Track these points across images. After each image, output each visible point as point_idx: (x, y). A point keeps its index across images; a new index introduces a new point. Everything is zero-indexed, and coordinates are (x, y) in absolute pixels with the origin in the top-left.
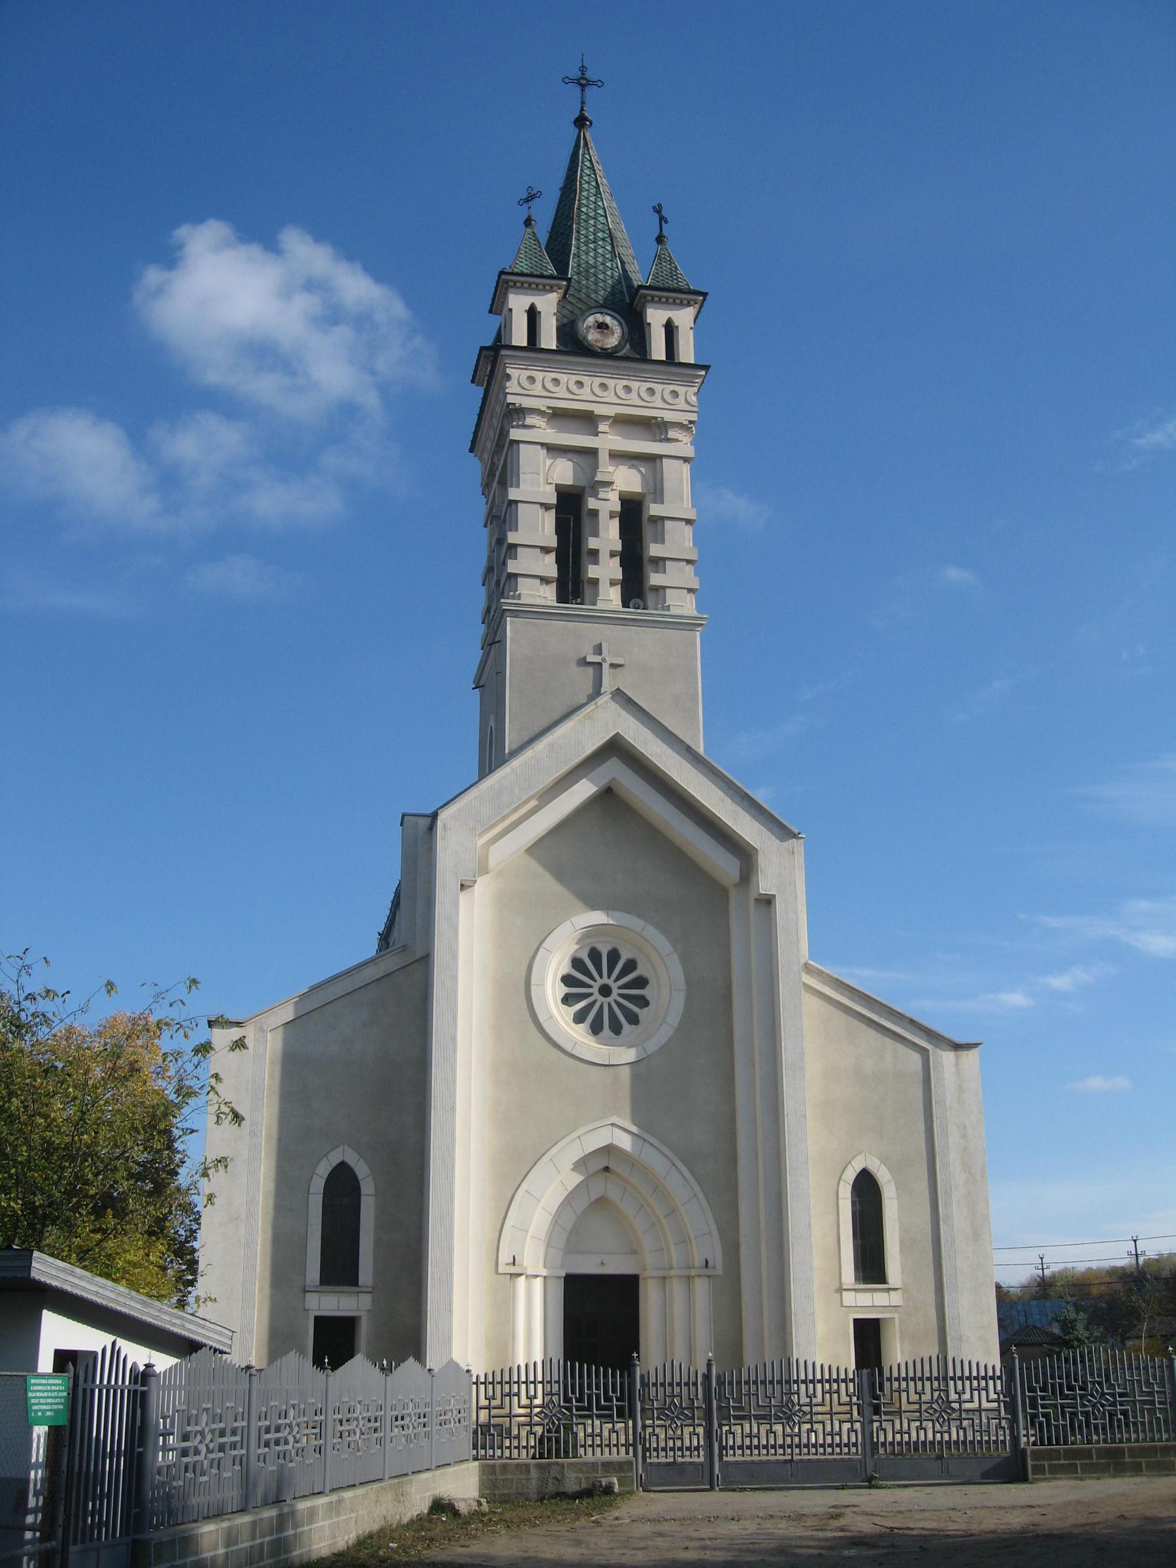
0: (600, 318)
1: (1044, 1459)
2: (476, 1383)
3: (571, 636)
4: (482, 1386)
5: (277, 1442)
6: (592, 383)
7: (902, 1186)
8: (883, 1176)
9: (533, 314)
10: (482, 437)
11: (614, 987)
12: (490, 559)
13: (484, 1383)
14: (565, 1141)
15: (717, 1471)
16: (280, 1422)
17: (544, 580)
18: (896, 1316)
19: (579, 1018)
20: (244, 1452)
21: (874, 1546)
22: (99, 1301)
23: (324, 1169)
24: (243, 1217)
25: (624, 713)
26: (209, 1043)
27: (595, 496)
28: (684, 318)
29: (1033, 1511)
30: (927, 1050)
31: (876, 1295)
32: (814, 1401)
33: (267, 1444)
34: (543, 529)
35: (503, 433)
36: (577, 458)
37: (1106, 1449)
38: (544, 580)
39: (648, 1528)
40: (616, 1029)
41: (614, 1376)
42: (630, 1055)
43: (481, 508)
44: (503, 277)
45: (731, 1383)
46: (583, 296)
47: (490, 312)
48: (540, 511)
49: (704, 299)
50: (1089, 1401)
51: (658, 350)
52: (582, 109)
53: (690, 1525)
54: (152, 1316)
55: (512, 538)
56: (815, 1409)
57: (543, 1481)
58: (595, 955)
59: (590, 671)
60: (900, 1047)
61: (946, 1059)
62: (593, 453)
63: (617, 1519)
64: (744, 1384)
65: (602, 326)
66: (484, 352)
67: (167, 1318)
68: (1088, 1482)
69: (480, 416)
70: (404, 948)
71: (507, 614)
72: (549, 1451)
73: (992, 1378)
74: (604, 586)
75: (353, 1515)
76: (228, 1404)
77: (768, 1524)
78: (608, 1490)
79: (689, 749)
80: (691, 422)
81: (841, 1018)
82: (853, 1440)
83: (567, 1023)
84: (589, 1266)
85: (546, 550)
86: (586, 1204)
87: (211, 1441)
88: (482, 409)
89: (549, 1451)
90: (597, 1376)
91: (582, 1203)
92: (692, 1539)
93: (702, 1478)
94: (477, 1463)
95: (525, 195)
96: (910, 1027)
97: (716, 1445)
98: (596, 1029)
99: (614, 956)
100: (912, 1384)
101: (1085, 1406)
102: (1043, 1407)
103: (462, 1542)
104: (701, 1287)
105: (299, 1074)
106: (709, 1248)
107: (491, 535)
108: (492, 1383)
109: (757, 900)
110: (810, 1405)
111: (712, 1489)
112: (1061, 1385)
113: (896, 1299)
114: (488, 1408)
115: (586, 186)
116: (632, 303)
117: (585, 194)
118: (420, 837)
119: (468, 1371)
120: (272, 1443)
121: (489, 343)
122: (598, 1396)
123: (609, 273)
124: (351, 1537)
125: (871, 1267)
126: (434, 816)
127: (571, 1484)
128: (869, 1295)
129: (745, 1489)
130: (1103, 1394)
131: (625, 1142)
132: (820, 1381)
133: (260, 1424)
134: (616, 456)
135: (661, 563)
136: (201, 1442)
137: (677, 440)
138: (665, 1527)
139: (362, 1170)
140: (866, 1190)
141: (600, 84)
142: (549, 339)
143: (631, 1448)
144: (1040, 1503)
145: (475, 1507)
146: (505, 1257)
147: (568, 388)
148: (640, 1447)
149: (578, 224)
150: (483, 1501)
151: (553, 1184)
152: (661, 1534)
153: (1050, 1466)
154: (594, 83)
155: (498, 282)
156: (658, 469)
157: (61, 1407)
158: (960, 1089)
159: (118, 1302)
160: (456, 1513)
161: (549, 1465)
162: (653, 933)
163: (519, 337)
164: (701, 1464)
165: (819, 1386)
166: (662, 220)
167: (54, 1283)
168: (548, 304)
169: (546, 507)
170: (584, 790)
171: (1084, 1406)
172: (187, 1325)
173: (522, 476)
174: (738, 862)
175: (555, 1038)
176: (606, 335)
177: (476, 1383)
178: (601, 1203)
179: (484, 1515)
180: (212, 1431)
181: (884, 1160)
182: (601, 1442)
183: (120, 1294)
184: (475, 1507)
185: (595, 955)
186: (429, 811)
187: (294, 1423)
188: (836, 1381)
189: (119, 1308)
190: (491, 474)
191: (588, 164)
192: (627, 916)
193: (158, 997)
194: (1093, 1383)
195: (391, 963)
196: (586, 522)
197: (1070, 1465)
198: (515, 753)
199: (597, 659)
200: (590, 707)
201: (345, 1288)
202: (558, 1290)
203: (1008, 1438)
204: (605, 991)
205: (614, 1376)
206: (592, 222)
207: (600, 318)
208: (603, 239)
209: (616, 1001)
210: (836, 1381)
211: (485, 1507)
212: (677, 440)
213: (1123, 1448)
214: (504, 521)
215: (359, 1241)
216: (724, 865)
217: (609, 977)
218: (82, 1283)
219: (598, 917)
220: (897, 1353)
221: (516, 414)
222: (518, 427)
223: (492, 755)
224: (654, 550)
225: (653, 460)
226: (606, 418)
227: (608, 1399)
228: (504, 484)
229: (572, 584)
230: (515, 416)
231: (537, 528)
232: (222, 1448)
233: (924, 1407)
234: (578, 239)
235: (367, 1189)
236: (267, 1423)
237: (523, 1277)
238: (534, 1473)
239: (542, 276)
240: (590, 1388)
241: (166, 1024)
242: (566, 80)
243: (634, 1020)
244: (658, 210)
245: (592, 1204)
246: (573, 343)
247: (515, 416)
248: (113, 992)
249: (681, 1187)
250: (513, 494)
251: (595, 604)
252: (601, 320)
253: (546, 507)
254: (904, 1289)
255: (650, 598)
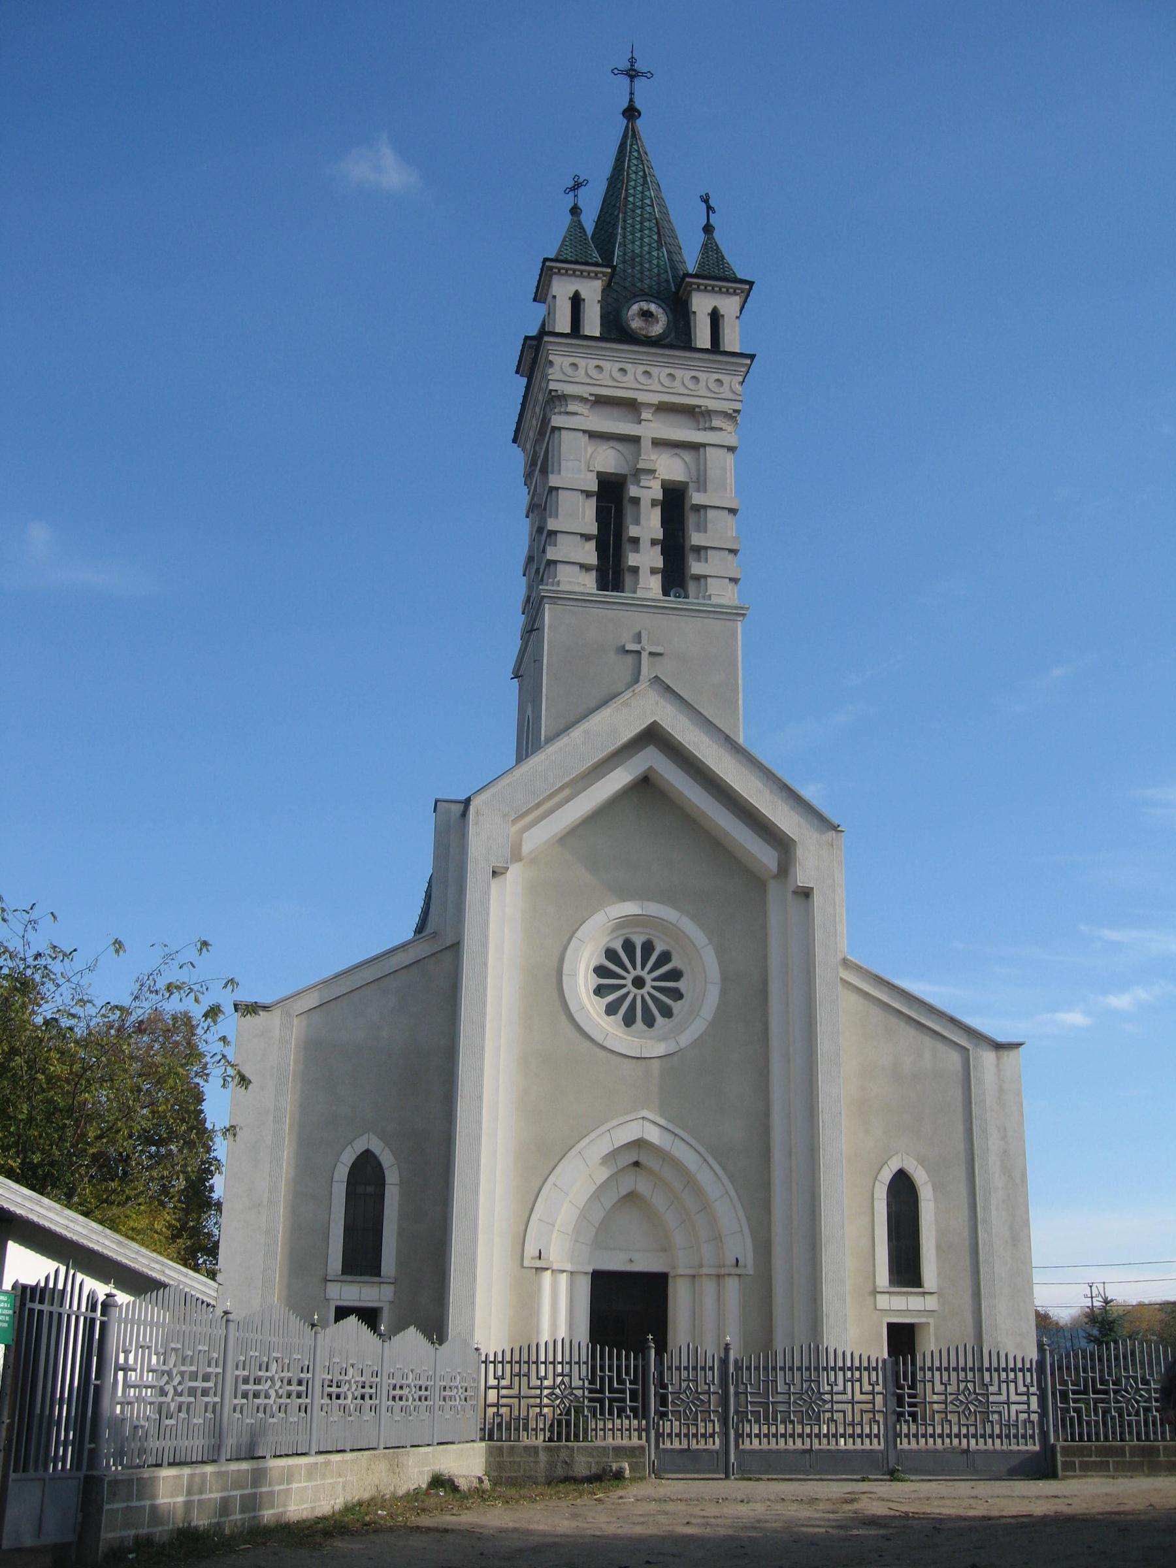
0: (645, 306)
1: (1074, 1455)
2: (485, 1362)
3: (613, 622)
4: (492, 1365)
5: (256, 1395)
6: (635, 372)
7: (939, 1188)
8: (920, 1177)
9: (577, 301)
10: (525, 425)
11: (648, 978)
12: (531, 548)
13: (493, 1362)
14: (593, 1135)
15: (732, 1459)
16: (260, 1373)
17: (585, 567)
18: (931, 1320)
19: (611, 1010)
20: (217, 1399)
21: (885, 1526)
22: (69, 1235)
23: (348, 1158)
24: (265, 1203)
25: (662, 701)
26: (218, 1007)
27: (638, 483)
28: (729, 305)
29: (1057, 1501)
30: (967, 1050)
31: (911, 1299)
32: (835, 1389)
33: (245, 1395)
34: (584, 517)
35: (545, 421)
36: (619, 446)
37: (1139, 1446)
38: (585, 567)
39: (653, 1506)
40: (650, 1022)
41: (627, 1358)
42: (660, 1049)
43: (522, 498)
44: (548, 264)
45: (749, 1368)
46: (627, 284)
47: (535, 300)
48: (581, 497)
49: (751, 288)
50: (1122, 1396)
51: (703, 339)
52: (631, 100)
53: (696, 1505)
54: (127, 1257)
55: (552, 525)
56: (836, 1398)
57: (552, 1465)
58: (628, 946)
59: (630, 660)
60: (941, 1047)
61: (988, 1057)
62: (636, 440)
63: (621, 1498)
64: (770, 1385)
65: (646, 315)
66: (528, 342)
67: (144, 1261)
68: (1120, 1480)
69: (523, 405)
70: (435, 935)
71: (545, 600)
72: (560, 1434)
73: (1021, 1370)
74: (644, 573)
75: (341, 1480)
76: (200, 1348)
77: (778, 1506)
78: (618, 1476)
79: (727, 738)
80: (735, 411)
81: (877, 1014)
82: (876, 1431)
83: (599, 1015)
84: (616, 1262)
85: (586, 537)
86: (616, 1199)
87: (180, 1383)
88: (525, 397)
89: (560, 1434)
90: (610, 1358)
91: (612, 1198)
92: (695, 1517)
93: (718, 1465)
94: (483, 1444)
95: (571, 184)
96: (951, 1026)
97: (732, 1432)
98: (629, 1021)
99: (648, 947)
100: (937, 1374)
101: (1119, 1402)
102: (1075, 1401)
103: (454, 1512)
104: (732, 1287)
105: (322, 1060)
106: (739, 1246)
107: (532, 525)
108: (502, 1362)
109: (795, 893)
110: (831, 1393)
111: (727, 1477)
112: (1094, 1379)
113: (931, 1303)
114: (497, 1387)
115: (633, 176)
116: (678, 291)
117: (632, 183)
118: (453, 819)
119: (477, 1349)
120: (251, 1395)
121: (533, 332)
122: (611, 1379)
123: (655, 262)
124: (339, 1503)
125: (906, 1269)
126: (467, 802)
127: (581, 1468)
128: (904, 1298)
129: (760, 1479)
130: (1138, 1390)
131: (654, 1135)
132: (842, 1369)
133: (237, 1373)
134: (658, 443)
135: (703, 552)
136: (167, 1383)
137: (721, 429)
138: (670, 1507)
139: (387, 1159)
140: (903, 1192)
141: (649, 75)
142: (592, 325)
143: (644, 1434)
144: (1066, 1494)
145: (476, 1483)
146: (531, 1251)
147: (611, 376)
148: (653, 1433)
149: (625, 213)
150: (485, 1478)
151: (579, 1179)
152: (666, 1513)
153: (1080, 1462)
154: (643, 75)
155: (542, 270)
156: (702, 457)
157: (5, 1325)
158: (1001, 1090)
159: (91, 1239)
160: (455, 1489)
161: (558, 1448)
162: (688, 926)
163: (563, 324)
164: (717, 1452)
165: (840, 1374)
166: (709, 208)
167: (19, 1211)
168: (592, 291)
169: (588, 494)
170: (620, 778)
171: (1118, 1402)
172: (167, 1271)
173: (563, 463)
174: (776, 854)
175: (587, 1029)
176: (651, 324)
177: (485, 1362)
178: (632, 1197)
179: (484, 1492)
180: (182, 1374)
181: (922, 1161)
182: (616, 1435)
183: (92, 1230)
184: (476, 1483)
185: (628, 946)
186: (463, 797)
187: (277, 1377)
188: (858, 1369)
189: (91, 1245)
190: (533, 464)
191: (635, 154)
192: (662, 907)
193: (169, 957)
194: (1127, 1378)
195: (423, 950)
196: (629, 510)
197: (1102, 1462)
198: (550, 740)
199: (636, 647)
200: (628, 694)
201: (366, 1278)
202: (585, 1285)
203: (1037, 1431)
204: (639, 983)
205: (627, 1358)
206: (638, 211)
207: (645, 306)
208: (650, 229)
209: (649, 993)
210: (858, 1369)
211: (487, 1484)
212: (721, 429)
213: (1158, 1447)
214: (545, 509)
215: (383, 1233)
216: (765, 856)
217: (643, 969)
218: (51, 1215)
219: (630, 908)
220: (929, 1345)
221: (556, 399)
222: (560, 413)
223: (528, 741)
224: (696, 539)
225: (695, 447)
226: (650, 405)
227: (621, 1381)
228: (545, 471)
229: (612, 573)
230: (557, 403)
231: (578, 515)
232: (192, 1392)
233: (950, 1398)
234: (624, 228)
235: (392, 1177)
236: (246, 1373)
237: (549, 1272)
238: (543, 1457)
239: (587, 264)
240: (602, 1370)
241: (179, 988)
242: (616, 72)
243: (667, 1013)
244: (706, 200)
245: (619, 1201)
246: (616, 331)
247: (557, 403)
248: (121, 952)
249: (712, 1182)
250: (554, 481)
251: (635, 592)
252: (645, 308)
253: (588, 494)
254: (939, 1294)
255: (692, 587)
